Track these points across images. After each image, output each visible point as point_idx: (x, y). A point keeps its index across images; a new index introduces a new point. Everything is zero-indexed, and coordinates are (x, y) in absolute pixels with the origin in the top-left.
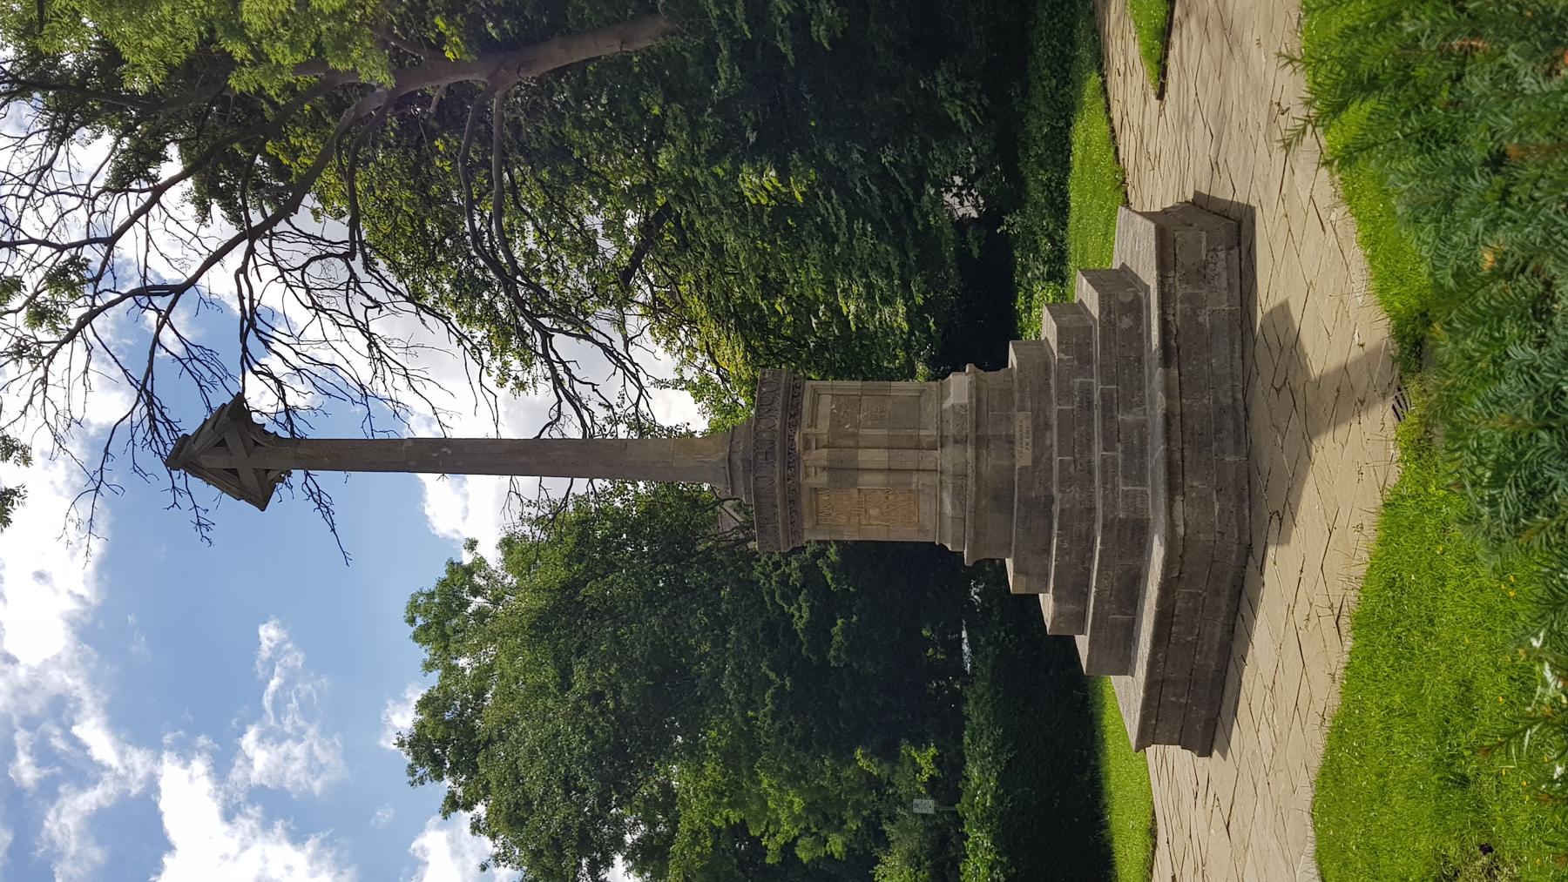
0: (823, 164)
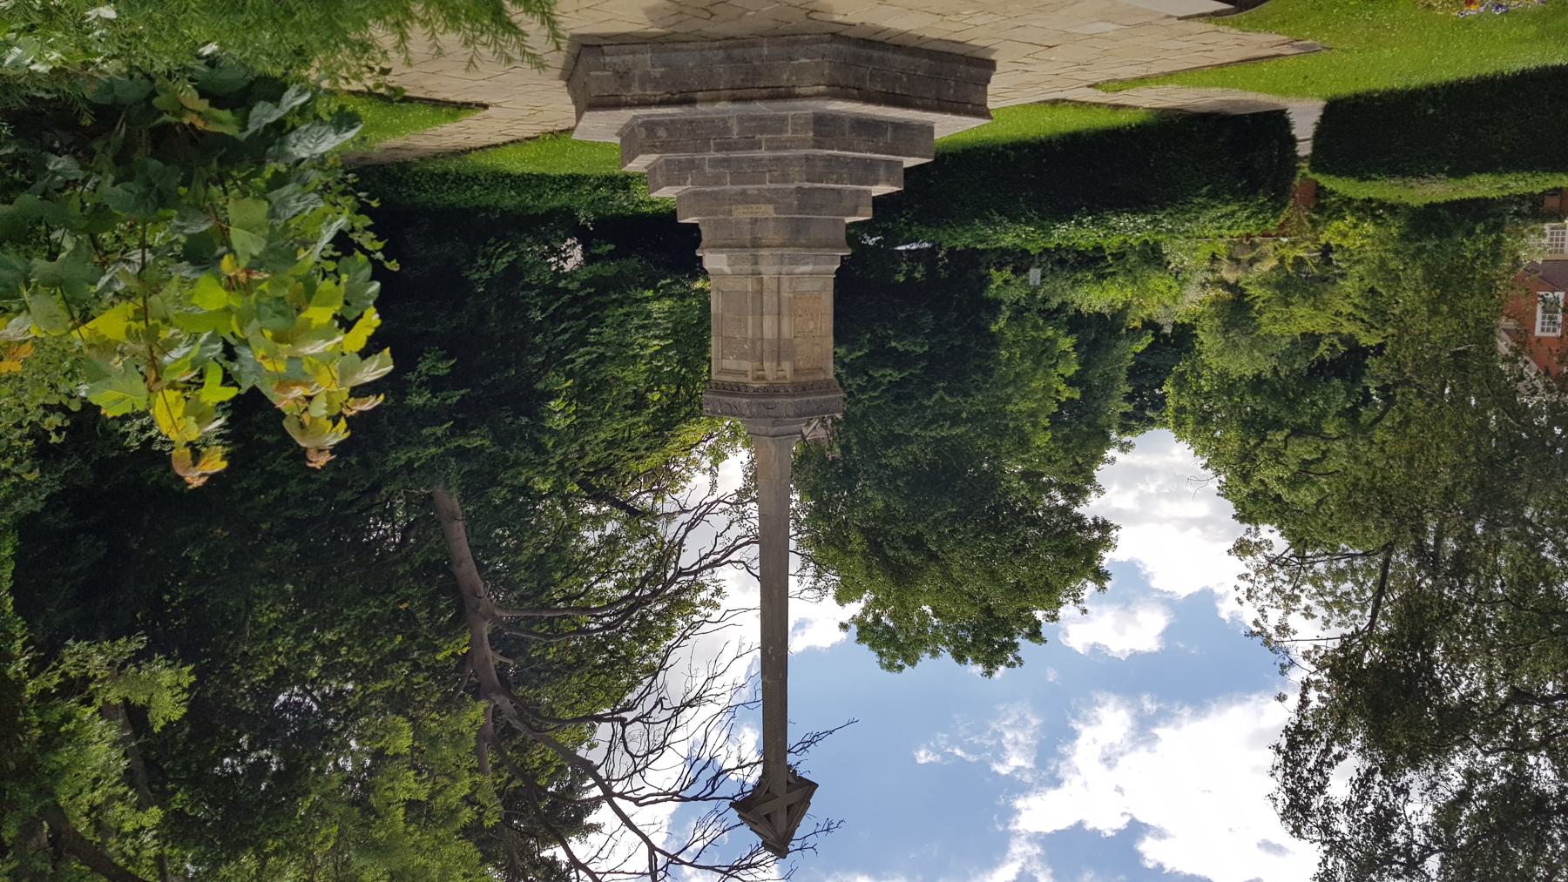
0: (544, 366)
